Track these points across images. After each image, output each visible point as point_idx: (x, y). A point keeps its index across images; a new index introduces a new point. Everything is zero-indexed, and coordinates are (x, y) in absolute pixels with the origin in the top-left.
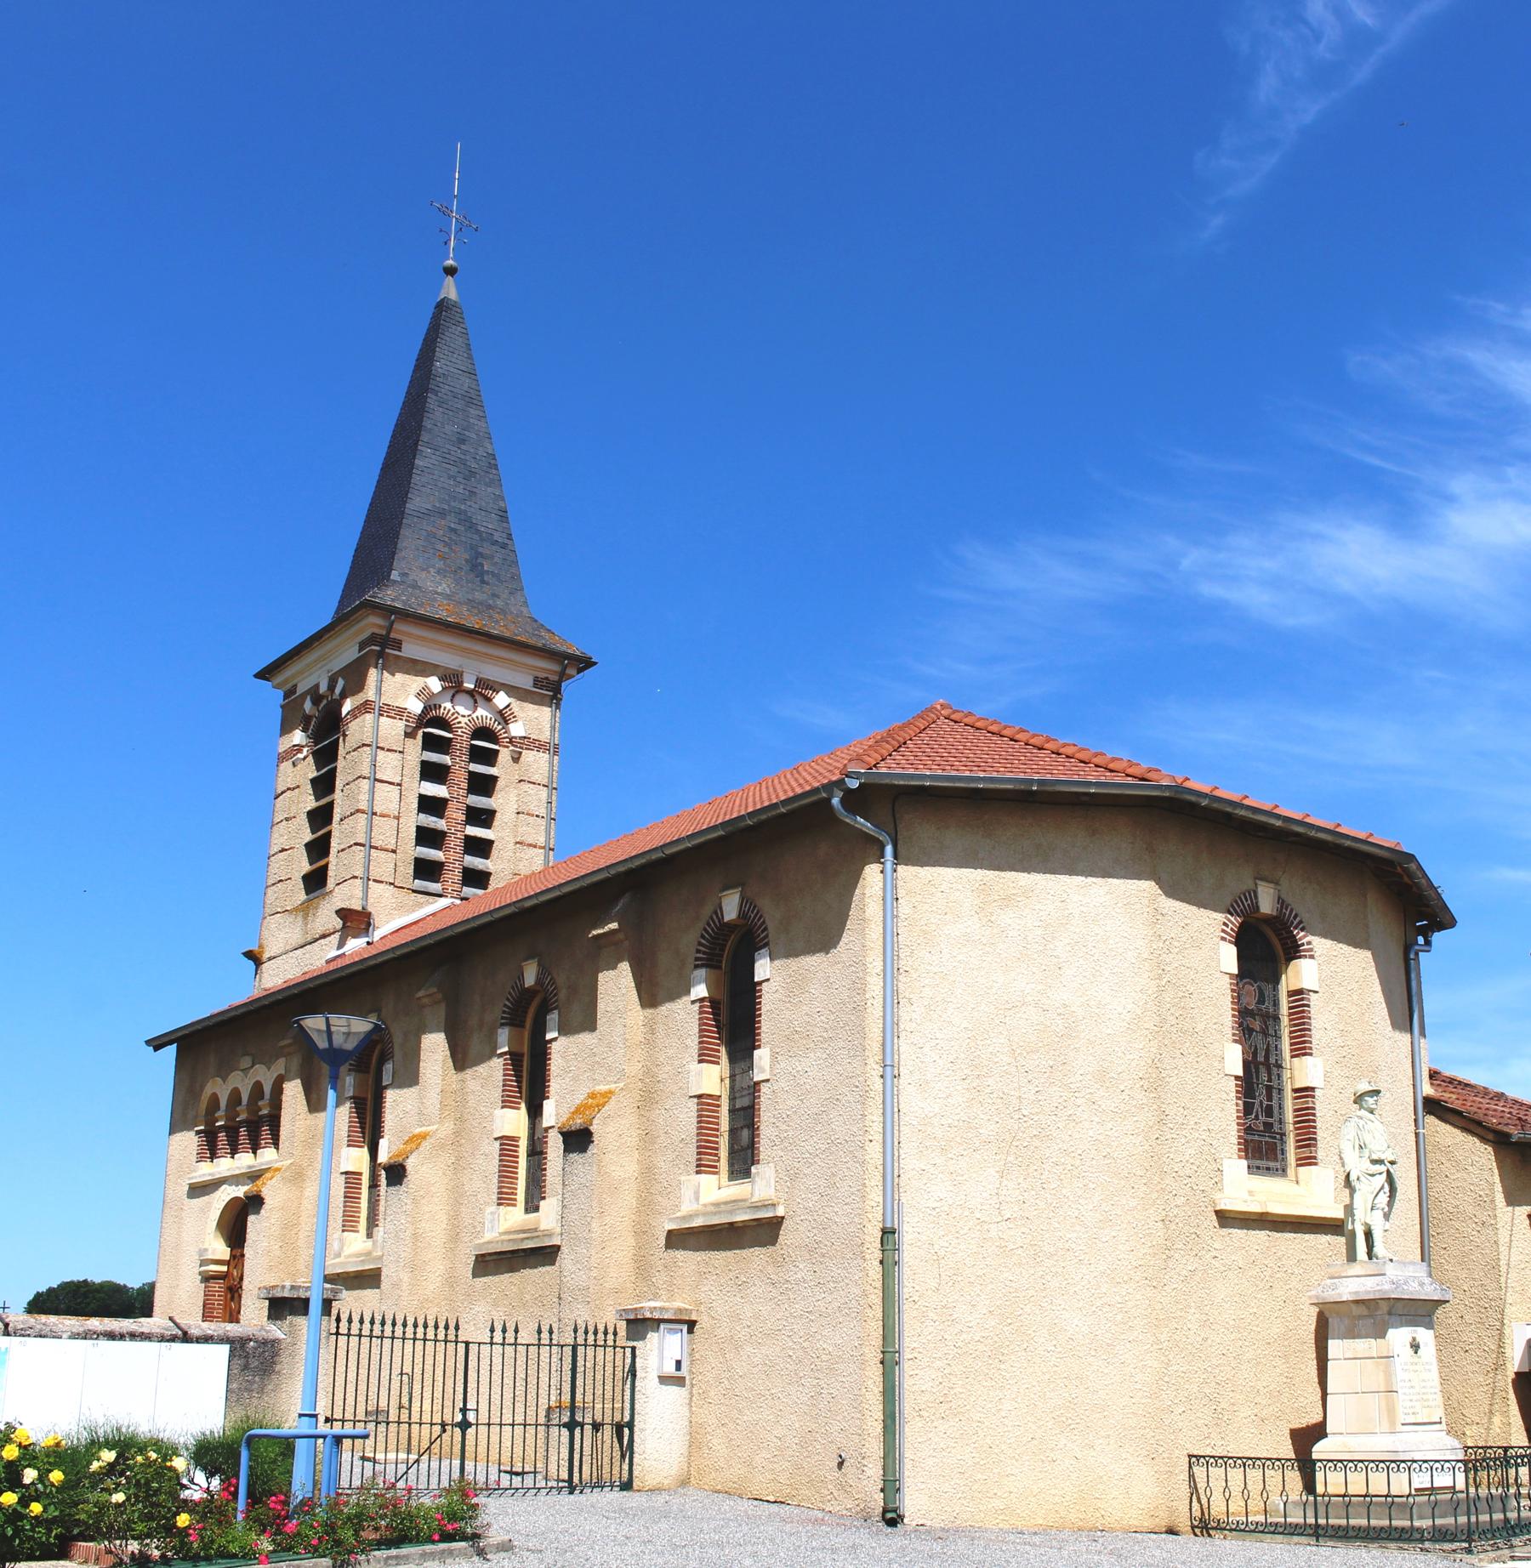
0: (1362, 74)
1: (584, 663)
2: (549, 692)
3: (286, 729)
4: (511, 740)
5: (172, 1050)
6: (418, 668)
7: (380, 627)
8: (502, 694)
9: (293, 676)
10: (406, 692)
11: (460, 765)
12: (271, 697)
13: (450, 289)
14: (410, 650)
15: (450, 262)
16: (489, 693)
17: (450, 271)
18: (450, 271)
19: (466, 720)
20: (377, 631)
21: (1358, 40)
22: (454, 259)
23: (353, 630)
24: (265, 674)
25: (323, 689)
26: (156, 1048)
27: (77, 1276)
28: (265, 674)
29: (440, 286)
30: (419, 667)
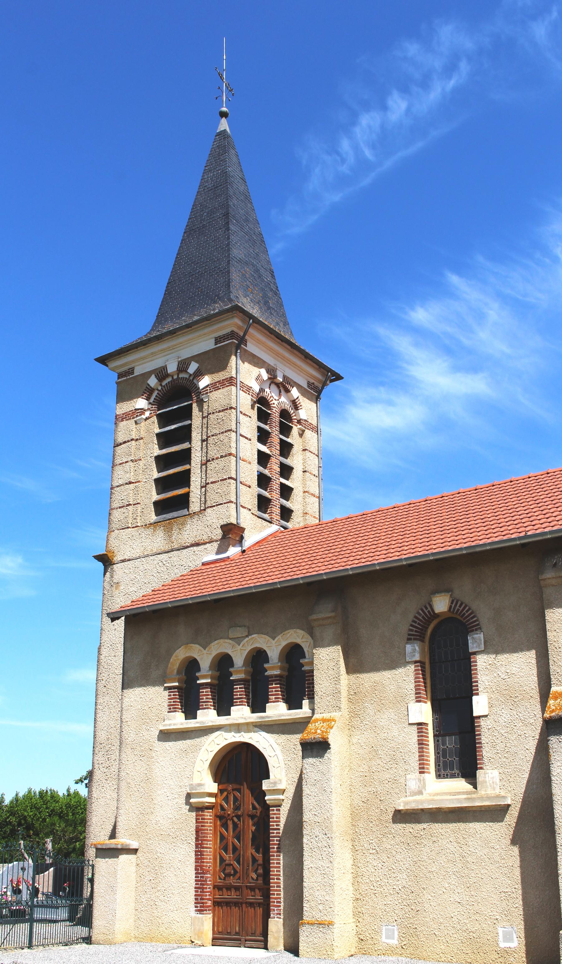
0: (366, 181)
1: (338, 377)
2: (315, 393)
3: (284, 377)
4: (299, 422)
5: (121, 622)
6: (256, 361)
7: (239, 328)
8: (295, 388)
9: (133, 361)
10: (249, 375)
11: (276, 436)
12: (108, 377)
13: (224, 125)
14: (251, 347)
15: (224, 109)
16: (289, 387)
17: (223, 115)
18: (223, 115)
19: (276, 402)
20: (235, 330)
21: (363, 166)
22: (226, 107)
23: (215, 327)
24: (103, 360)
25: (172, 368)
26: (113, 620)
27: (38, 786)
28: (103, 360)
29: (218, 123)
30: (256, 360)
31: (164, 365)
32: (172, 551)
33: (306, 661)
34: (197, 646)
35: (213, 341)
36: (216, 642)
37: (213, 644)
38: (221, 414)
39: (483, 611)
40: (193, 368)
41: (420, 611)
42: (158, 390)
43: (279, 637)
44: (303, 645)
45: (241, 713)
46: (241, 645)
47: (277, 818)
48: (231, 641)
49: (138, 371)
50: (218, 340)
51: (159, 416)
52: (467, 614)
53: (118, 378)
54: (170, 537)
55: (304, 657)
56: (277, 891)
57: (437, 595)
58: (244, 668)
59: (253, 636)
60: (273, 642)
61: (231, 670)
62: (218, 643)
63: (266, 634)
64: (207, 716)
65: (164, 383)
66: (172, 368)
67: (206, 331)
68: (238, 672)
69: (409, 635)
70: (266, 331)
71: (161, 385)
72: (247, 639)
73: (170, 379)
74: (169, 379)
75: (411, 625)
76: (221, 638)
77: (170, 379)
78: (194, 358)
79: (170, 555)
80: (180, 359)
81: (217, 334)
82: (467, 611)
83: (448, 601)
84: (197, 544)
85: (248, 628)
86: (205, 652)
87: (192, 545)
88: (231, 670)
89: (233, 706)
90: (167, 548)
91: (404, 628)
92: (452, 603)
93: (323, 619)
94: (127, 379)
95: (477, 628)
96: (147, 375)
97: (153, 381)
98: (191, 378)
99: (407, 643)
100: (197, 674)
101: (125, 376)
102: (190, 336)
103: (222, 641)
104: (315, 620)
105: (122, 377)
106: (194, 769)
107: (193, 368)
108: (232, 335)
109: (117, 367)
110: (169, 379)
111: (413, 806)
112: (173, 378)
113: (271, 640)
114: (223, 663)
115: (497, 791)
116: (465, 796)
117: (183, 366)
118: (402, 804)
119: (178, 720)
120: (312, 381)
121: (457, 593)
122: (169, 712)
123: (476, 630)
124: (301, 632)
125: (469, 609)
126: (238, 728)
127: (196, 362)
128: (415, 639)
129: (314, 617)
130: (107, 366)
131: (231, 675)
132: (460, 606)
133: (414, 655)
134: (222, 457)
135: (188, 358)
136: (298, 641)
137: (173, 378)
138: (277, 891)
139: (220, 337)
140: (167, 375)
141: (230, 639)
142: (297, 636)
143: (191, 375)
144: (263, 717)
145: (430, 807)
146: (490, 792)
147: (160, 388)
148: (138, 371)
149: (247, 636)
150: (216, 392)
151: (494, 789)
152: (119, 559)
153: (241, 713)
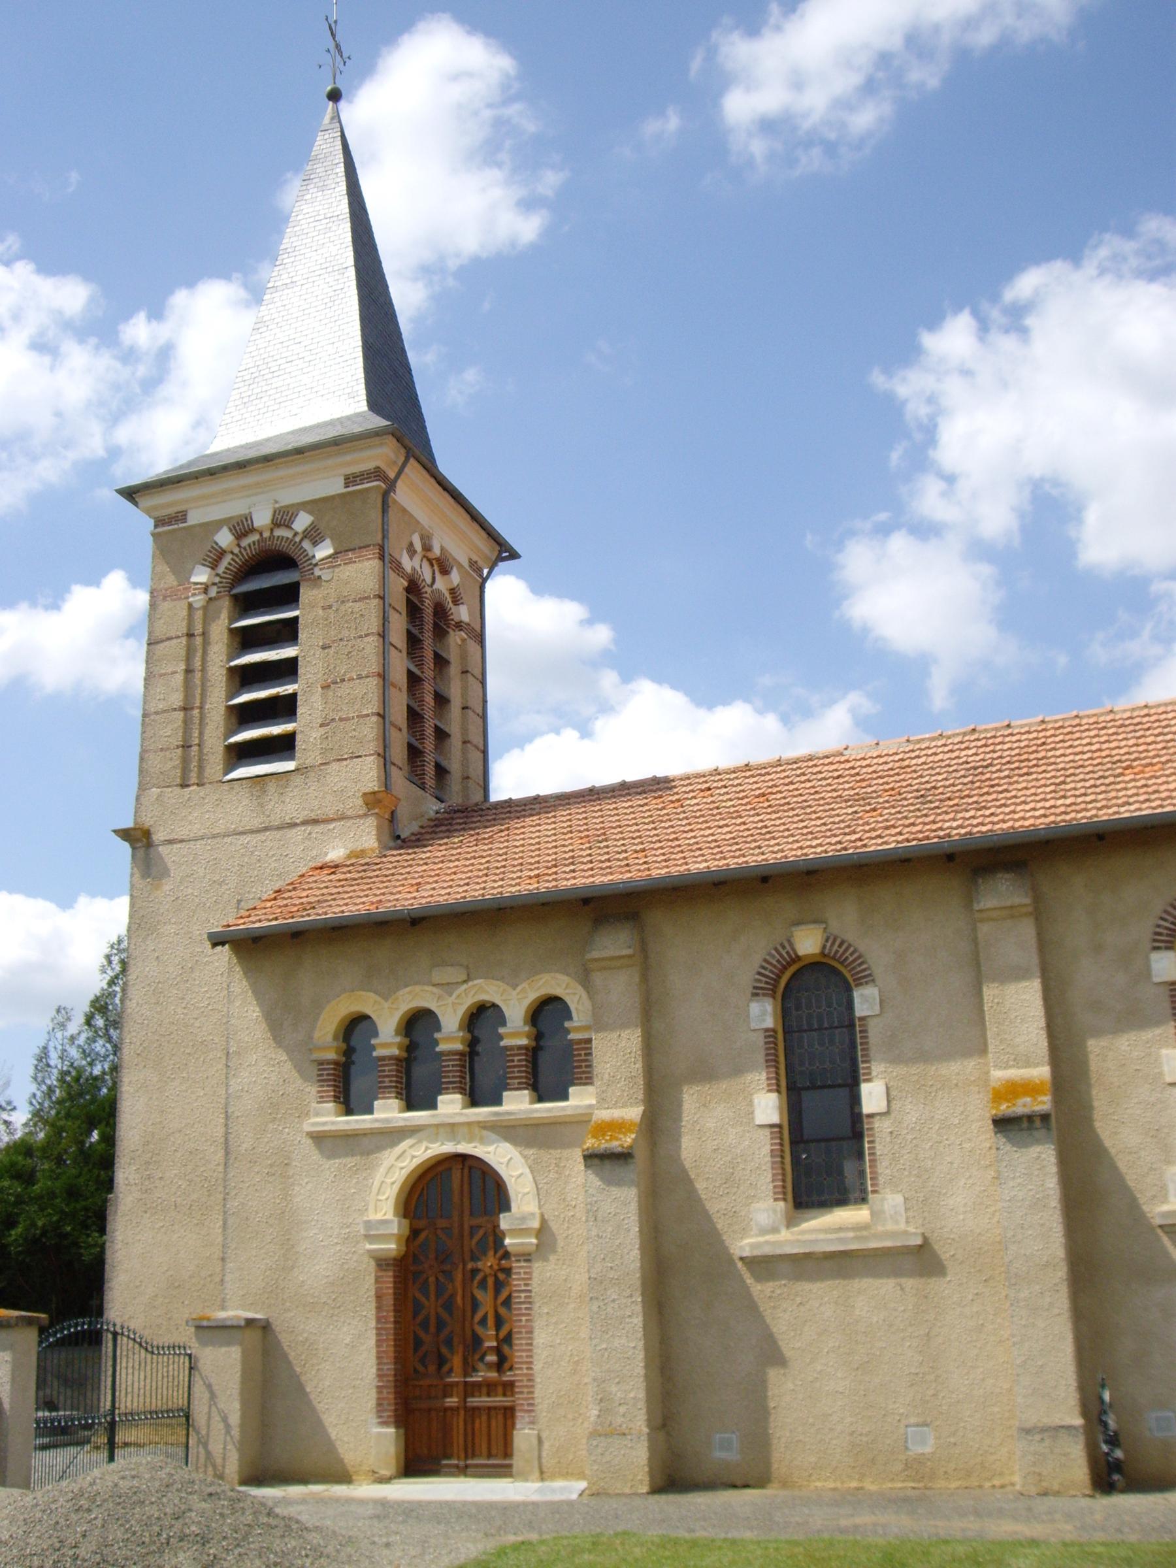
3: (442, 549)
20: (383, 466)
23: (348, 458)
25: (262, 519)
31: (247, 512)
32: (266, 829)
33: (575, 1024)
34: (372, 994)
35: (342, 481)
36: (408, 989)
37: (401, 992)
38: (358, 604)
39: (877, 951)
40: (302, 521)
41: (774, 952)
42: (232, 553)
43: (525, 985)
44: (567, 999)
45: (451, 1105)
46: (454, 996)
47: (525, 1273)
48: (435, 990)
49: (194, 518)
50: (349, 480)
51: (236, 598)
52: (851, 959)
53: (156, 526)
54: (261, 805)
55: (570, 1018)
56: (527, 1386)
57: (803, 927)
58: (461, 1034)
59: (476, 982)
60: (514, 993)
61: (437, 1035)
62: (410, 993)
63: (502, 979)
64: (388, 1111)
65: (245, 542)
66: (262, 519)
67: (330, 462)
68: (449, 1039)
69: (755, 988)
70: (291, 458)
71: (239, 545)
72: (465, 986)
73: (256, 537)
74: (255, 537)
75: (759, 973)
76: (416, 983)
77: (256, 537)
78: (310, 506)
79: (261, 837)
80: (277, 506)
81: (350, 470)
82: (851, 954)
83: (820, 937)
84: (315, 822)
85: (467, 967)
86: (386, 1005)
87: (305, 823)
88: (437, 1035)
89: (441, 1094)
90: (256, 823)
91: (747, 976)
92: (827, 941)
93: (612, 958)
94: (174, 530)
95: (865, 978)
96: (217, 525)
97: (225, 538)
98: (297, 539)
99: (751, 1000)
100: (373, 1042)
101: (170, 524)
102: (299, 469)
103: (418, 988)
104: (596, 960)
105: (163, 525)
106: (376, 1198)
107: (302, 521)
108: (378, 474)
109: (155, 508)
110: (255, 537)
111: (767, 1250)
112: (261, 534)
113: (509, 989)
114: (419, 1024)
115: (902, 1226)
116: (851, 1234)
117: (283, 518)
118: (747, 1249)
119: (329, 1118)
120: (475, 558)
121: (835, 926)
122: (319, 1102)
123: (867, 983)
124: (564, 979)
125: (855, 951)
126: (451, 1129)
127: (310, 513)
128: (764, 995)
129: (595, 954)
130: (136, 504)
131: (437, 1044)
132: (840, 946)
133: (764, 1020)
134: (360, 677)
135: (293, 505)
136: (558, 992)
137: (261, 534)
138: (527, 1386)
139: (355, 476)
140: (252, 530)
141: (434, 985)
142: (557, 983)
143: (296, 534)
144: (497, 1114)
145: (794, 1251)
146: (890, 1227)
147: (236, 550)
148: (194, 518)
149: (465, 982)
150: (349, 567)
151: (897, 1222)
152: (162, 839)
153: (451, 1105)
